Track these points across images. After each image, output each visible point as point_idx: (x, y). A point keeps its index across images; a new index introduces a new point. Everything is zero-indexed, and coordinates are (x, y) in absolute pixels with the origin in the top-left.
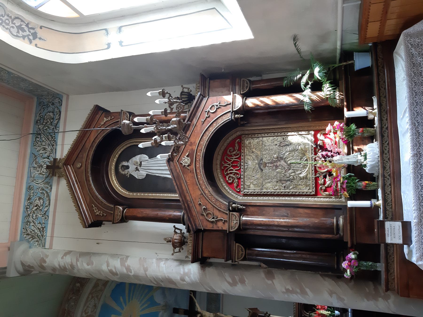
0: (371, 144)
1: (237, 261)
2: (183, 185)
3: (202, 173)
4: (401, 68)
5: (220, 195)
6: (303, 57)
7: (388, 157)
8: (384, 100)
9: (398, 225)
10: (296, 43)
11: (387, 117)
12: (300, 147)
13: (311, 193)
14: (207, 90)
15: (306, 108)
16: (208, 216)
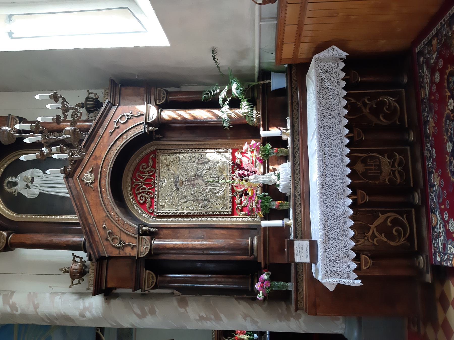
0: (284, 164)
1: (146, 291)
2: (84, 206)
3: (108, 192)
4: (312, 91)
5: (129, 217)
6: (222, 72)
7: (299, 178)
8: (296, 122)
9: (306, 243)
10: (215, 56)
11: (299, 138)
12: (218, 165)
13: (227, 213)
14: (117, 97)
15: (224, 125)
16: (113, 240)
